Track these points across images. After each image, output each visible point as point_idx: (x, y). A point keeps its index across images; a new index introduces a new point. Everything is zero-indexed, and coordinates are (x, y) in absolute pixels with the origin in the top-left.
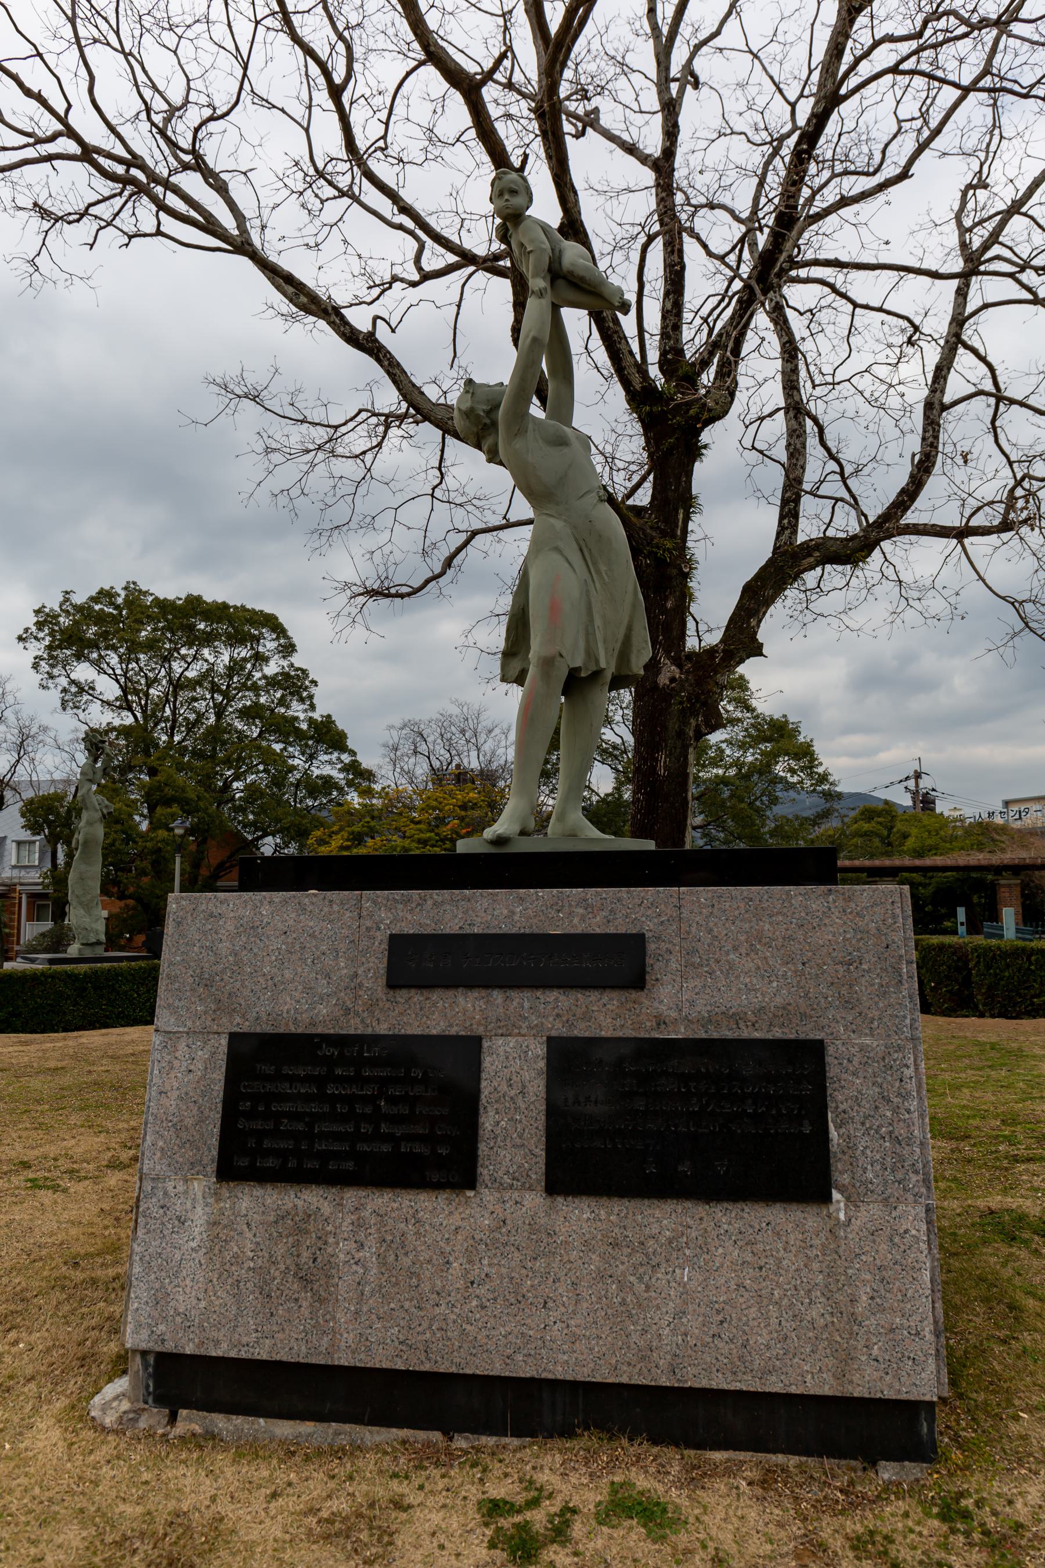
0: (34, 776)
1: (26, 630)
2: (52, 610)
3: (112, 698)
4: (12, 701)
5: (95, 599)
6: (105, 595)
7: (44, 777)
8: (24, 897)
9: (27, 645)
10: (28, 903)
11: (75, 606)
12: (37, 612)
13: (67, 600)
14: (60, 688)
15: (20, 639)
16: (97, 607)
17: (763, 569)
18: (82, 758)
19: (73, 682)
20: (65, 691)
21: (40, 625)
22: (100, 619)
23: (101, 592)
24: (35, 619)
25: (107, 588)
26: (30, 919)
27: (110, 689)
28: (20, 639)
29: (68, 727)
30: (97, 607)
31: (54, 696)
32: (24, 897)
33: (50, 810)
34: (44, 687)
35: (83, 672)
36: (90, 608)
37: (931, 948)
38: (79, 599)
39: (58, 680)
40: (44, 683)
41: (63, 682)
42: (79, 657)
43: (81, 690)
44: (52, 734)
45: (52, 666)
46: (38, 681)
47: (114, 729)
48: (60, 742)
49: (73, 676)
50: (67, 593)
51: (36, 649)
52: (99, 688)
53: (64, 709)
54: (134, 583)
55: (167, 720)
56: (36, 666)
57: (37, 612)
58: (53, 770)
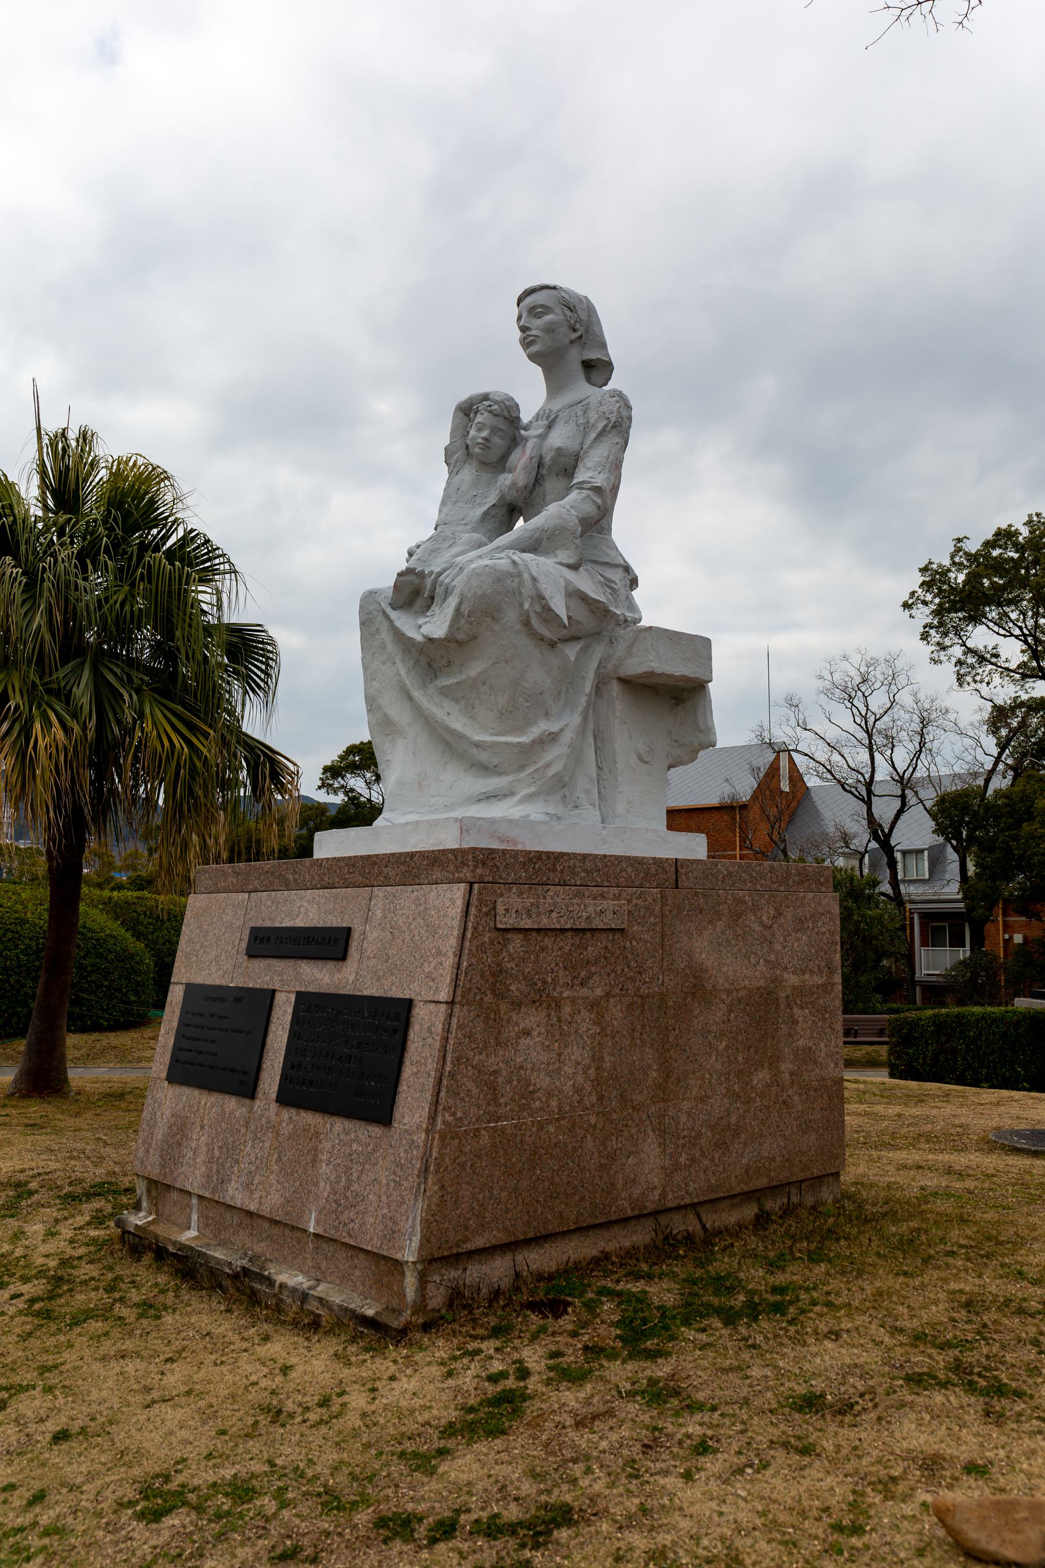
0: (933, 768)
1: (913, 593)
2: (940, 566)
3: (1013, 666)
4: (904, 682)
5: (989, 545)
6: (1005, 536)
7: (944, 771)
8: (916, 916)
9: (913, 612)
10: (921, 925)
11: (967, 554)
12: (924, 570)
13: (958, 550)
14: (954, 660)
15: (906, 606)
16: (995, 553)
17: (337, 828)
18: (990, 744)
19: (970, 651)
20: (960, 663)
21: (927, 585)
22: (997, 566)
23: (999, 533)
24: (921, 579)
25: (1004, 526)
26: (924, 943)
27: (1013, 652)
28: (906, 606)
29: (969, 707)
30: (995, 553)
31: (949, 669)
32: (916, 916)
33: (965, 809)
34: (935, 661)
35: (981, 637)
36: (988, 556)
37: (924, 999)
38: (973, 546)
39: (950, 651)
40: (935, 655)
41: (957, 651)
42: (976, 618)
43: (982, 659)
44: (952, 717)
45: (945, 634)
46: (928, 655)
47: (1022, 704)
48: (961, 725)
49: (970, 644)
50: (959, 540)
51: (923, 615)
52: (1004, 654)
53: (961, 685)
54: (1038, 515)
55: (216, 884)
56: (925, 636)
57: (924, 570)
58: (953, 761)
